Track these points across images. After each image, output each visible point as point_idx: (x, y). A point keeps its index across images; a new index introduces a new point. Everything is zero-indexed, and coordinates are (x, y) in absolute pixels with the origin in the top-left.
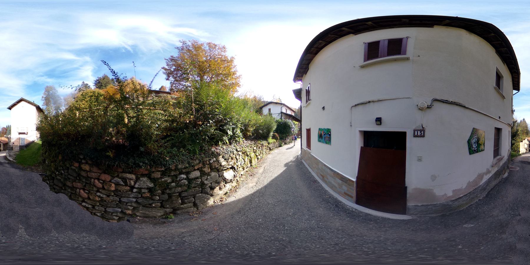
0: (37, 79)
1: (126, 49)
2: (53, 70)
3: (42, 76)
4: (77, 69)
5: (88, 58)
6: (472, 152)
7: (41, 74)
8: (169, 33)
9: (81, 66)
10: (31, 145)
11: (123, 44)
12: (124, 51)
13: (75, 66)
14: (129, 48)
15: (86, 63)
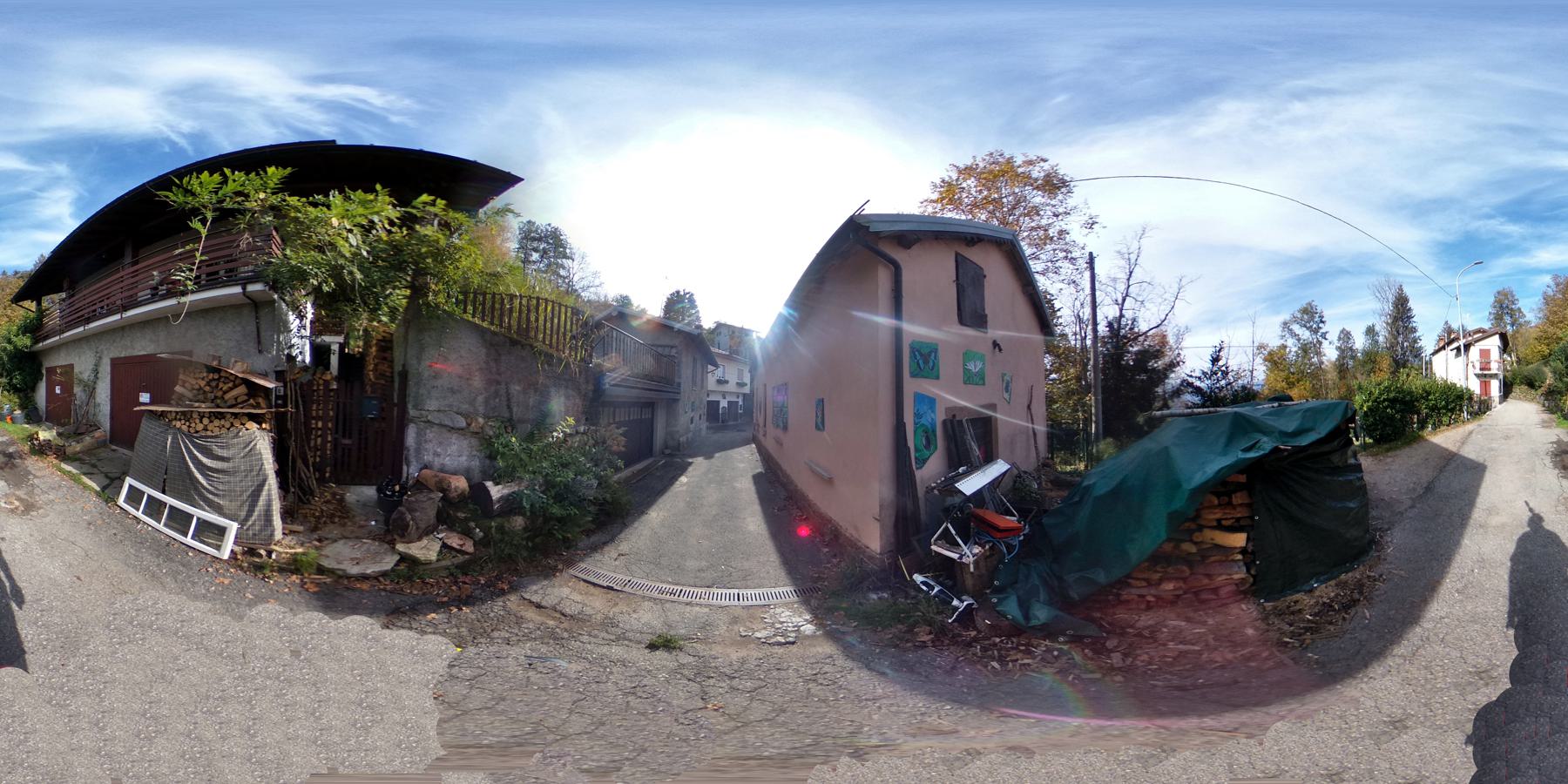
0: (1475, 225)
1: (173, 144)
2: (1524, 201)
3: (1489, 217)
4: (29, 196)
5: (61, 169)
6: (817, 428)
7: (1486, 210)
8: (301, 99)
9: (41, 189)
10: (1223, 440)
11: (165, 129)
12: (167, 149)
13: (22, 189)
14: (183, 142)
15: (56, 181)
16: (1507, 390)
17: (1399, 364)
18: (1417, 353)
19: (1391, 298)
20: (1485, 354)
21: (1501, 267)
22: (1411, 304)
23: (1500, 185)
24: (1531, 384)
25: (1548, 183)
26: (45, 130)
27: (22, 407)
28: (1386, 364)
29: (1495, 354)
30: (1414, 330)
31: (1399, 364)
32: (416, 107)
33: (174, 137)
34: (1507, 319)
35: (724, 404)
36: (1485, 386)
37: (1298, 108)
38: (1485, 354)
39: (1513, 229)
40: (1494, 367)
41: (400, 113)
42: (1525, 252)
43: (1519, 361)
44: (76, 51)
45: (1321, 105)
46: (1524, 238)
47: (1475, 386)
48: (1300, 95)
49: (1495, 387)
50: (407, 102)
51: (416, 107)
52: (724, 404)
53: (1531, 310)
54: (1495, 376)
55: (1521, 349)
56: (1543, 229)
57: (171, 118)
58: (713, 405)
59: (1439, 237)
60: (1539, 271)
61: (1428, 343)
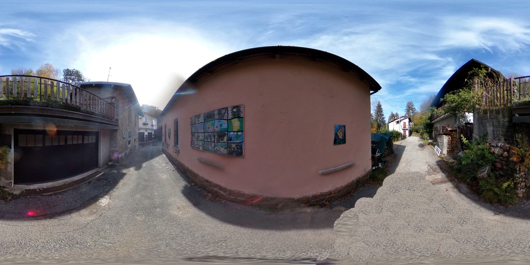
0: (400, 78)
1: (486, 50)
2: (416, 70)
3: (405, 76)
5: (450, 59)
7: (404, 73)
8: (526, 34)
9: (444, 66)
11: (483, 45)
13: (438, 66)
14: (489, 49)
15: (448, 63)
16: (411, 134)
17: (379, 126)
18: (384, 122)
19: (377, 105)
20: (405, 123)
21: (409, 92)
22: (382, 107)
23: (409, 65)
24: (417, 132)
25: (423, 64)
26: (444, 46)
27: (429, 136)
28: (375, 125)
29: (407, 124)
30: (383, 115)
31: (379, 126)
32: (34, 35)
33: (486, 48)
34: (411, 111)
35: (146, 133)
36: (405, 132)
37: (346, 38)
38: (405, 123)
39: (413, 80)
40: (407, 127)
41: (29, 38)
42: (416, 87)
43: (414, 125)
44: (450, 20)
45: (353, 37)
46: (416, 83)
47: (402, 132)
48: (347, 34)
49: (407, 133)
50: (31, 34)
51: (34, 35)
52: (146, 133)
53: (417, 108)
54: (407, 129)
55: (415, 121)
56: (422, 80)
57: (484, 41)
58: (141, 135)
59: (389, 82)
60: (419, 94)
61: (387, 120)
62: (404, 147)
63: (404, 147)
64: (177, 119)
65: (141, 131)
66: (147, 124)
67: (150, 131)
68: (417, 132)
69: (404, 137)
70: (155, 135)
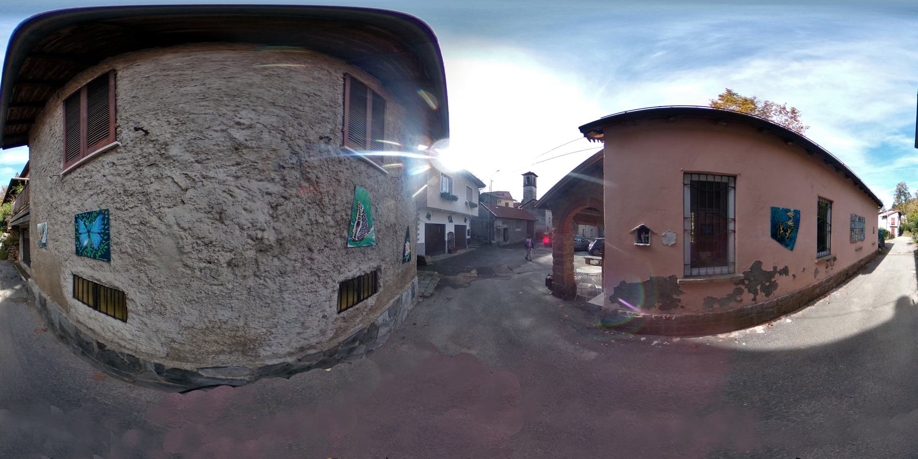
3: (896, 134)
16: (901, 233)
20: (893, 219)
34: (903, 198)
36: (893, 230)
37: (796, 66)
38: (893, 219)
47: (889, 230)
48: (798, 59)
52: (450, 228)
62: (893, 245)
63: (893, 245)
64: (583, 129)
65: (435, 220)
66: (455, 199)
67: (461, 223)
68: (910, 231)
69: (892, 237)
70: (472, 233)
